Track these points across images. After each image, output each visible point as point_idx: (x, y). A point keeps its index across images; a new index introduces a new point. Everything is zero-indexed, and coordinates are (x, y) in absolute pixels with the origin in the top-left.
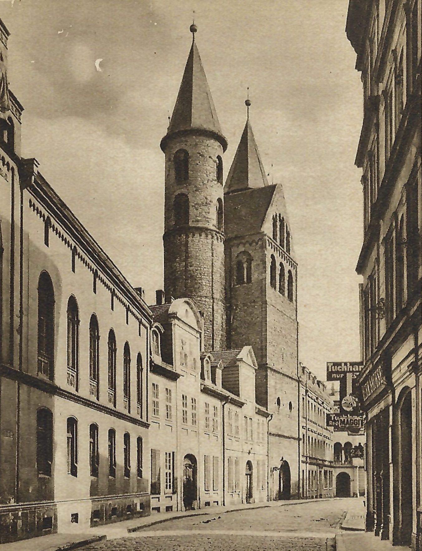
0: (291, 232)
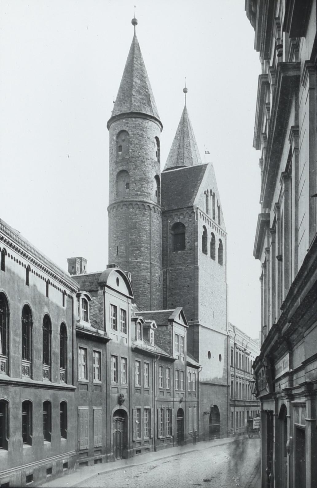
0: (222, 208)
